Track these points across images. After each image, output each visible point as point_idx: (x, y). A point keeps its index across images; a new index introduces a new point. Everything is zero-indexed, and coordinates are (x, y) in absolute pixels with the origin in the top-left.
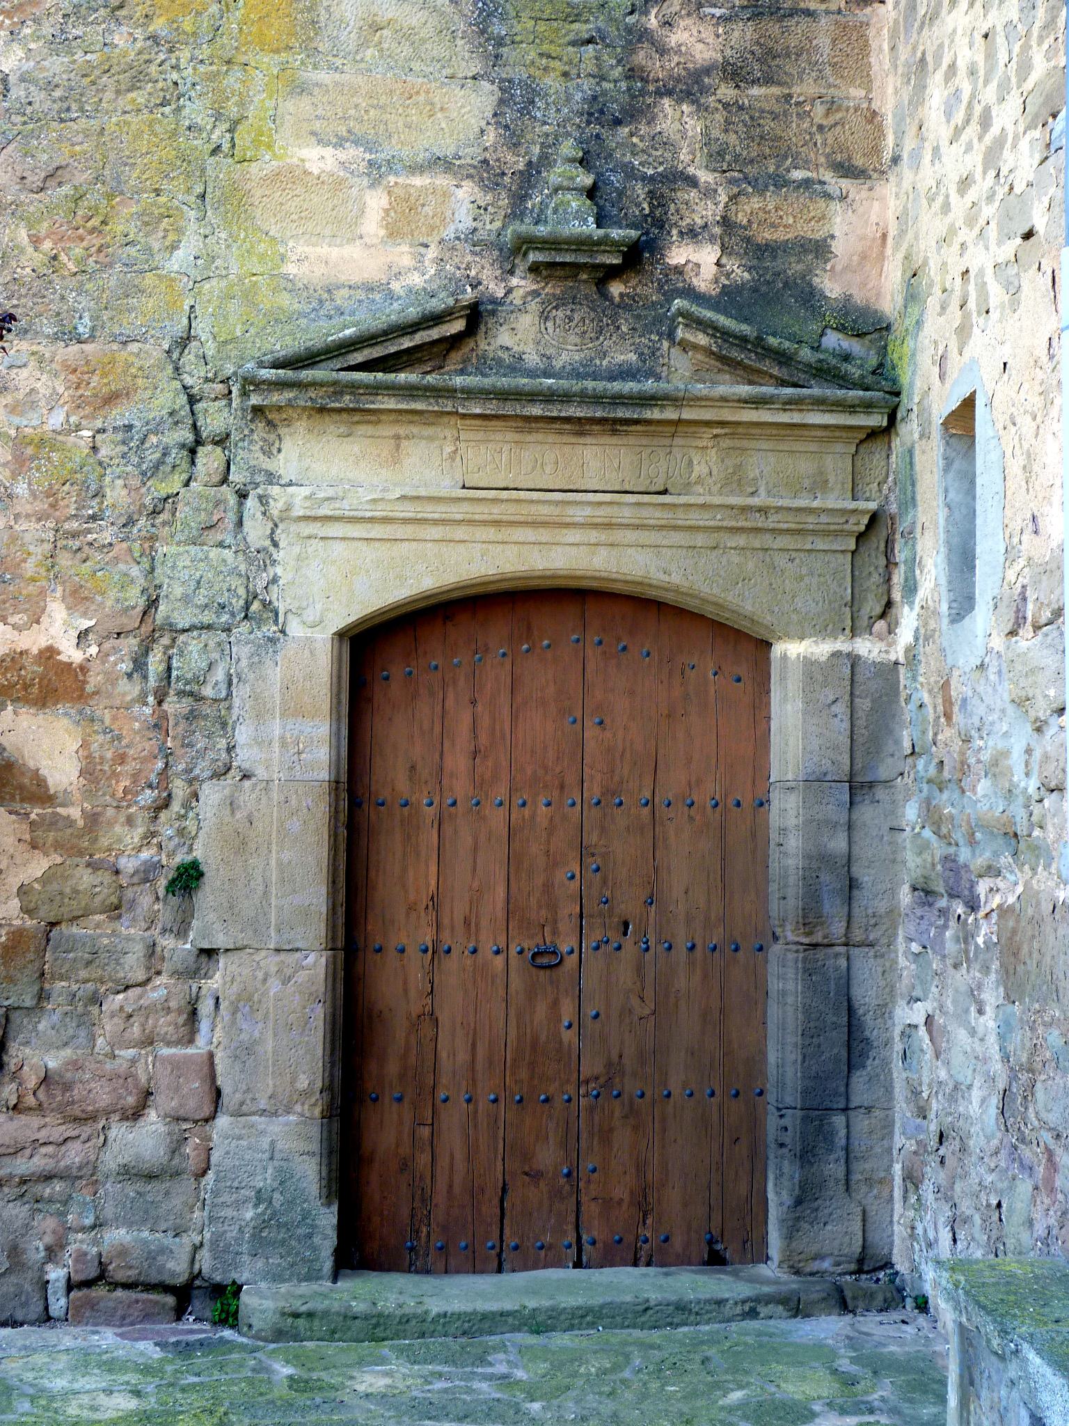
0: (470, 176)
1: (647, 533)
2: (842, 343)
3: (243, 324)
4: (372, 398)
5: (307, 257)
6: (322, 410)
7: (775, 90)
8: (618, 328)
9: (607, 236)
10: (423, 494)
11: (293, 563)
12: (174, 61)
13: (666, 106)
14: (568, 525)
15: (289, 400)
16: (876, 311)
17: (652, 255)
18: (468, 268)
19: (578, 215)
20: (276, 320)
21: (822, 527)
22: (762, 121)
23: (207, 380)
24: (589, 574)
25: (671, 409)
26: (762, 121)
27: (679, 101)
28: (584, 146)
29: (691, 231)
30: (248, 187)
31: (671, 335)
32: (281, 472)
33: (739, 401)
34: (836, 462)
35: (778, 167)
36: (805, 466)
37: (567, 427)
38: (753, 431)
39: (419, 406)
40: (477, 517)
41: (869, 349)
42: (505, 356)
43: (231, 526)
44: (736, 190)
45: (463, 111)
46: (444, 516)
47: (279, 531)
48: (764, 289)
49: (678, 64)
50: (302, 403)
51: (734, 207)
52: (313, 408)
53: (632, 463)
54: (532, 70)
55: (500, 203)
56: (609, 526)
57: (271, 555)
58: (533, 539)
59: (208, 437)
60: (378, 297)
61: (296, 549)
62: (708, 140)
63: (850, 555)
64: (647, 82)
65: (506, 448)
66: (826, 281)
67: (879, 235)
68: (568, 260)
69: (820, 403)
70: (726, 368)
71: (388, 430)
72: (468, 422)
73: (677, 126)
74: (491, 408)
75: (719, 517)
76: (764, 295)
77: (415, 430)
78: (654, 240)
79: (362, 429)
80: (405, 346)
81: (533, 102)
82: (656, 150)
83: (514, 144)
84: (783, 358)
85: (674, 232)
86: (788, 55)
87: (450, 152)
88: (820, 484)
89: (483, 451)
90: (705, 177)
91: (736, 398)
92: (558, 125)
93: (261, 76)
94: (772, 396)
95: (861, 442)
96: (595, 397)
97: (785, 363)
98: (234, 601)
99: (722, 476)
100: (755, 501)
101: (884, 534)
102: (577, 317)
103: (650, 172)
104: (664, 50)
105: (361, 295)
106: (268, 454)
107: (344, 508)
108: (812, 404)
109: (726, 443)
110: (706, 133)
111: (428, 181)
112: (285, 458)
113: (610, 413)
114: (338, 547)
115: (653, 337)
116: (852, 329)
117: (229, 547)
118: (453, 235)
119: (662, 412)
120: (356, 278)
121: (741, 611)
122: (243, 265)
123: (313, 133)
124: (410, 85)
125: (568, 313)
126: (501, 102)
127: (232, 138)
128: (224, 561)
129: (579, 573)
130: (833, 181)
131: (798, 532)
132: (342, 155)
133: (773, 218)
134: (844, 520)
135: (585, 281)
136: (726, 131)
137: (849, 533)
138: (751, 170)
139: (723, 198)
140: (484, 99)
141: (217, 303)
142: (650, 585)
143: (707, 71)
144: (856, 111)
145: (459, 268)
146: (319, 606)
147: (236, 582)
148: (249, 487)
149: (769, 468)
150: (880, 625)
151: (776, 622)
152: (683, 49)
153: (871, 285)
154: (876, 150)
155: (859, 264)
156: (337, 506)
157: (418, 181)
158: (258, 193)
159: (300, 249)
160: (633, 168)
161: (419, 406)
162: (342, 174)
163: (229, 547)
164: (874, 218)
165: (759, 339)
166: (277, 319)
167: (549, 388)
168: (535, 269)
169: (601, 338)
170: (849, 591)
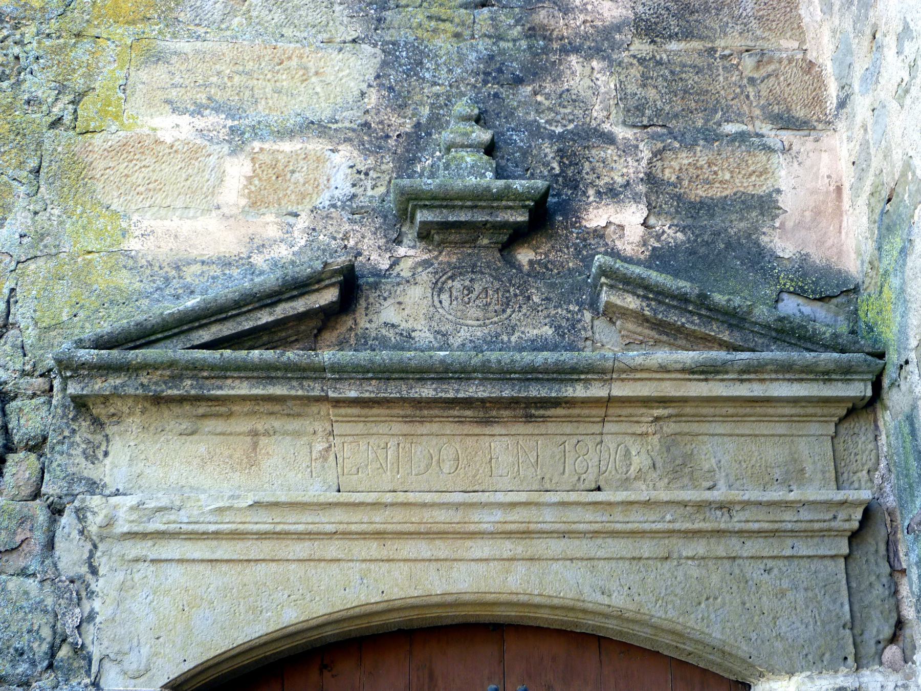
0: (348, 140)
1: (577, 542)
2: (803, 309)
3: (72, 306)
4: (219, 382)
5: (153, 232)
6: (158, 400)
7: (696, 44)
8: (529, 298)
9: (508, 187)
10: (283, 499)
11: (113, 594)
12: (18, 37)
13: (574, 63)
14: (472, 535)
15: (115, 388)
16: (840, 271)
17: (566, 218)
18: (346, 237)
19: (474, 170)
20: (111, 302)
21: (803, 526)
22: (684, 75)
23: (24, 374)
24: (503, 598)
25: (598, 384)
26: (684, 75)
27: (588, 58)
28: (481, 106)
29: (611, 190)
30: (89, 159)
31: (593, 304)
32: (107, 480)
33: (683, 371)
34: (812, 446)
35: (707, 121)
36: (773, 453)
37: (468, 413)
38: (704, 411)
39: (278, 390)
40: (353, 528)
41: (837, 315)
42: (390, 334)
43: (38, 548)
44: (660, 145)
45: (340, 75)
46: (310, 527)
47: (98, 554)
48: (702, 250)
49: (584, 22)
50: (131, 391)
51: (659, 164)
52: (146, 398)
53: (553, 456)
54: (419, 33)
55: (383, 167)
56: (526, 534)
57: (88, 586)
58: (428, 555)
59: (20, 442)
60: (235, 272)
61: (120, 576)
62: (622, 94)
63: (841, 562)
64: (551, 40)
65: (392, 443)
66: (776, 240)
67: (832, 188)
68: (463, 219)
69: (786, 370)
70: (664, 338)
71: (243, 425)
72: (343, 411)
73: (587, 82)
74: (370, 390)
75: (668, 517)
76: (705, 257)
77: (277, 424)
78: (567, 201)
79: (210, 425)
80: (264, 321)
81: (421, 63)
82: (564, 107)
83: (400, 106)
84: (735, 319)
85: (591, 192)
86: (707, 10)
87: (325, 115)
88: (795, 474)
89: (363, 447)
90: (622, 133)
91: (679, 366)
92: (451, 86)
93: (113, 47)
94: (725, 363)
95: (842, 420)
96: (502, 372)
97: (737, 326)
98: (35, 645)
99: (669, 468)
100: (716, 495)
101: (883, 533)
102: (478, 287)
103: (559, 130)
104: (568, 9)
105: (215, 270)
106: (91, 458)
107: (182, 520)
108: (776, 372)
109: (670, 428)
110: (621, 88)
111: (300, 146)
112: (112, 463)
113: (520, 396)
114: (175, 572)
115: (571, 307)
116: (813, 292)
117: (34, 575)
118: (327, 203)
119: (587, 388)
120: (210, 252)
121: (707, 640)
122: (76, 242)
123: (168, 102)
124: (281, 51)
125: (467, 283)
126: (384, 64)
127: (75, 111)
128: (26, 593)
130: (773, 133)
131: (773, 533)
132: (200, 123)
133: (707, 173)
134: (831, 516)
135: (486, 247)
136: (644, 86)
137: (839, 533)
138: (677, 125)
139: (646, 154)
140: (364, 61)
141: (42, 285)
142: (585, 611)
143: (618, 28)
144: (790, 63)
145: (335, 239)
146: (145, 651)
147: (40, 621)
148: (65, 500)
149: (727, 457)
150: (892, 652)
151: (755, 653)
152: (589, 7)
153: (829, 243)
154: (818, 100)
155: (814, 220)
156: (172, 518)
157: (287, 146)
158: (100, 165)
159: (145, 223)
160: (539, 126)
161: (278, 390)
162: (199, 141)
163: (34, 575)
164: (824, 171)
165: (703, 297)
166: (111, 300)
167: (442, 361)
168: (425, 235)
169: (509, 311)
170: (847, 607)
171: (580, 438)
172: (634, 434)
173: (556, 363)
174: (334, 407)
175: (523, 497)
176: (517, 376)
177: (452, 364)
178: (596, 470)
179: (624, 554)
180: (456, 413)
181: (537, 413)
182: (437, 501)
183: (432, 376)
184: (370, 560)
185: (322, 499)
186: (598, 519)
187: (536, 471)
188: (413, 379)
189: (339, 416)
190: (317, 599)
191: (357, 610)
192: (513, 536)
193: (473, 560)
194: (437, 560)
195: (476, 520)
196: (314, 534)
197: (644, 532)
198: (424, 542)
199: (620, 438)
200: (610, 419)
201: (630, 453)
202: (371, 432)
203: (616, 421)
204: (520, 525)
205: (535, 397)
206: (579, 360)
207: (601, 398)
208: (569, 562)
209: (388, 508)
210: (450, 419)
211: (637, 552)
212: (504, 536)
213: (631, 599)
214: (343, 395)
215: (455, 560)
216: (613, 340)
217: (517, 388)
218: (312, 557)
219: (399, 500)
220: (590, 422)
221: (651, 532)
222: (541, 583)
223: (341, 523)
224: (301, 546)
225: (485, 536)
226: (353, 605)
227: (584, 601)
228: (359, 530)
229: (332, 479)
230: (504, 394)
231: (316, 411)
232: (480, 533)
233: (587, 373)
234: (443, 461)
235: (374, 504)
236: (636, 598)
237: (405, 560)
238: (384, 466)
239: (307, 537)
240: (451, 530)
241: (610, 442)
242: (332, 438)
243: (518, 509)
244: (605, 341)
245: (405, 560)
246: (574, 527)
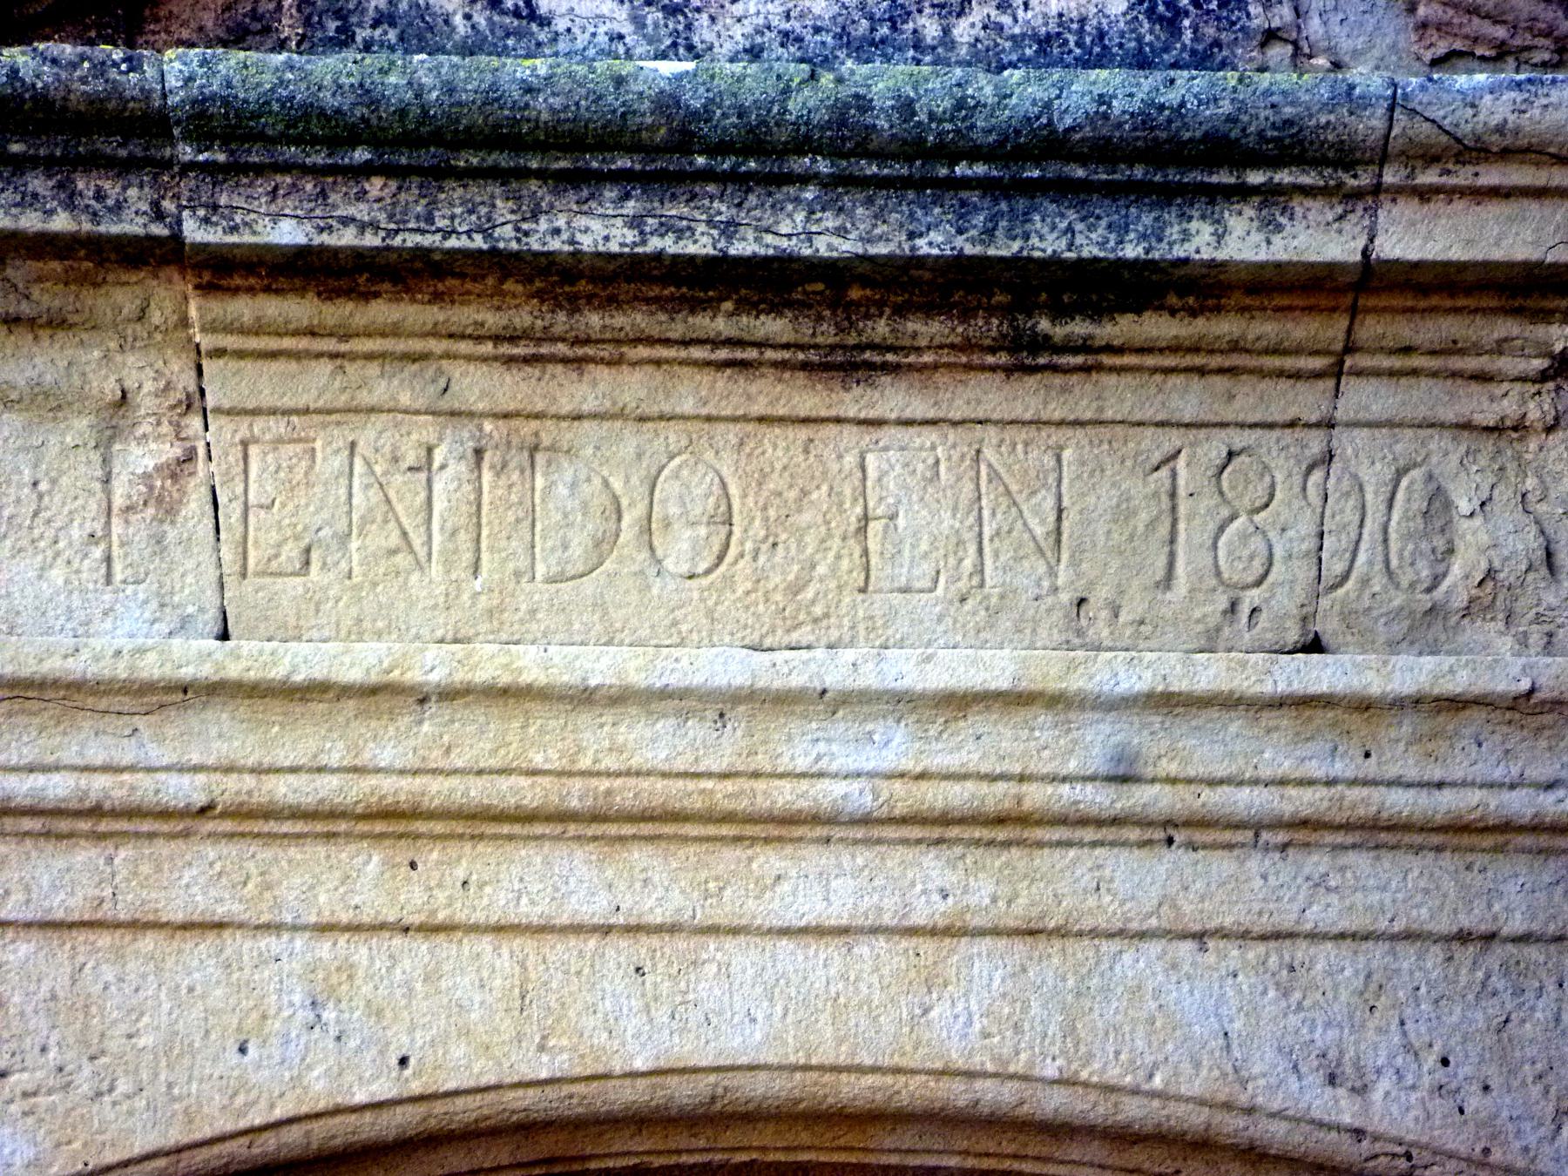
1: (1223, 865)
24: (912, 1092)
25: (1320, 212)
37: (773, 326)
40: (283, 789)
46: (99, 785)
53: (1123, 513)
56: (1009, 826)
58: (595, 908)
72: (243, 308)
74: (358, 220)
89: (330, 463)
96: (913, 147)
119: (1271, 226)
129: (854, 1090)
167: (667, 103)
171: (1240, 439)
172: (1466, 426)
173: (1144, 119)
174: (206, 289)
175: (996, 668)
176: (980, 169)
177: (706, 114)
178: (1304, 572)
179: (1422, 916)
180: (721, 325)
181: (1059, 332)
182: (638, 679)
183: (623, 162)
184: (354, 928)
185: (151, 668)
186: (1316, 769)
187: (1052, 573)
188: (542, 175)
189: (228, 329)
190: (123, 1086)
191: (293, 1135)
192: (954, 832)
193: (785, 932)
194: (634, 929)
195: (802, 764)
196: (115, 814)
197: (1507, 827)
198: (579, 853)
199: (1406, 443)
200: (1363, 361)
201: (1448, 505)
202: (365, 398)
203: (1392, 373)
204: (984, 788)
205: (1055, 262)
206: (1242, 107)
207: (1332, 268)
208: (1187, 947)
209: (432, 707)
210: (697, 353)
211: (1479, 908)
212: (916, 832)
213: (1449, 1105)
214: (247, 238)
215: (713, 930)
216: (1382, 44)
217: (979, 219)
218: (106, 912)
219: (481, 676)
220: (1281, 374)
221: (1536, 827)
222: (1069, 1031)
223: (229, 769)
224: (60, 863)
225: (837, 832)
226: (278, 1113)
227: (1250, 1111)
228: (308, 800)
229: (193, 584)
230: (923, 246)
231: (130, 308)
232: (815, 819)
233: (1275, 163)
234: (667, 525)
235: (372, 691)
236: (1474, 1102)
237: (499, 929)
238: (417, 541)
239: (84, 825)
240: (697, 804)
241: (1366, 460)
242: (195, 422)
243: (977, 722)
244: (1345, 45)
245: (499, 929)
246: (1213, 799)
